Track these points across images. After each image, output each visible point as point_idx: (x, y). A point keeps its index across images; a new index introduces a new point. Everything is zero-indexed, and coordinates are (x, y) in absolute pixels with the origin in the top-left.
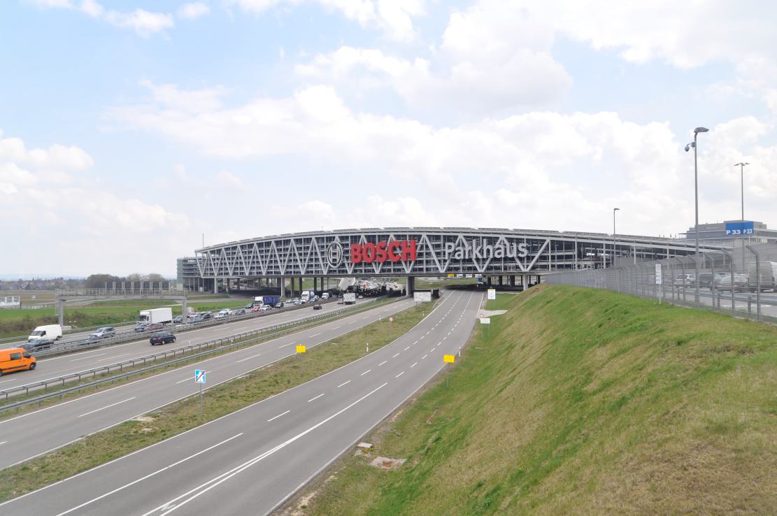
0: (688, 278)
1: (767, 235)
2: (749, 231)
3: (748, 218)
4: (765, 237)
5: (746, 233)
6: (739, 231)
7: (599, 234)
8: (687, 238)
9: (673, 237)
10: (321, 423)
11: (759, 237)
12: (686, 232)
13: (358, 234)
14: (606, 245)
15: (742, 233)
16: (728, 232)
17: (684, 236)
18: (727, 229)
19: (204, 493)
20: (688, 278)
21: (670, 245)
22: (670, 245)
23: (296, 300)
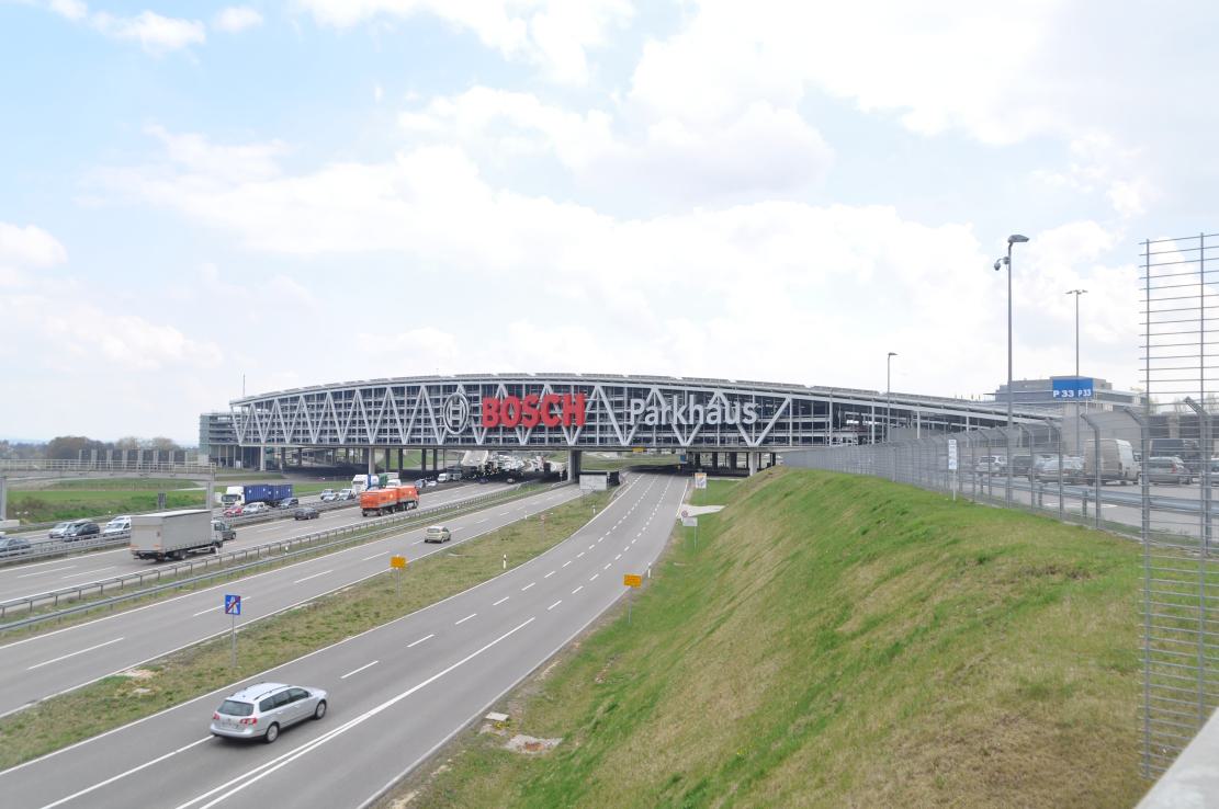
0: (997, 461)
1: (1113, 400)
2: (1087, 393)
3: (1084, 373)
5: (1082, 396)
6: (1072, 392)
7: (912, 396)
11: (1101, 402)
12: (994, 392)
15: (1076, 394)
16: (1056, 393)
17: (993, 398)
20: (997, 461)
21: (690, 386)
22: (690, 386)
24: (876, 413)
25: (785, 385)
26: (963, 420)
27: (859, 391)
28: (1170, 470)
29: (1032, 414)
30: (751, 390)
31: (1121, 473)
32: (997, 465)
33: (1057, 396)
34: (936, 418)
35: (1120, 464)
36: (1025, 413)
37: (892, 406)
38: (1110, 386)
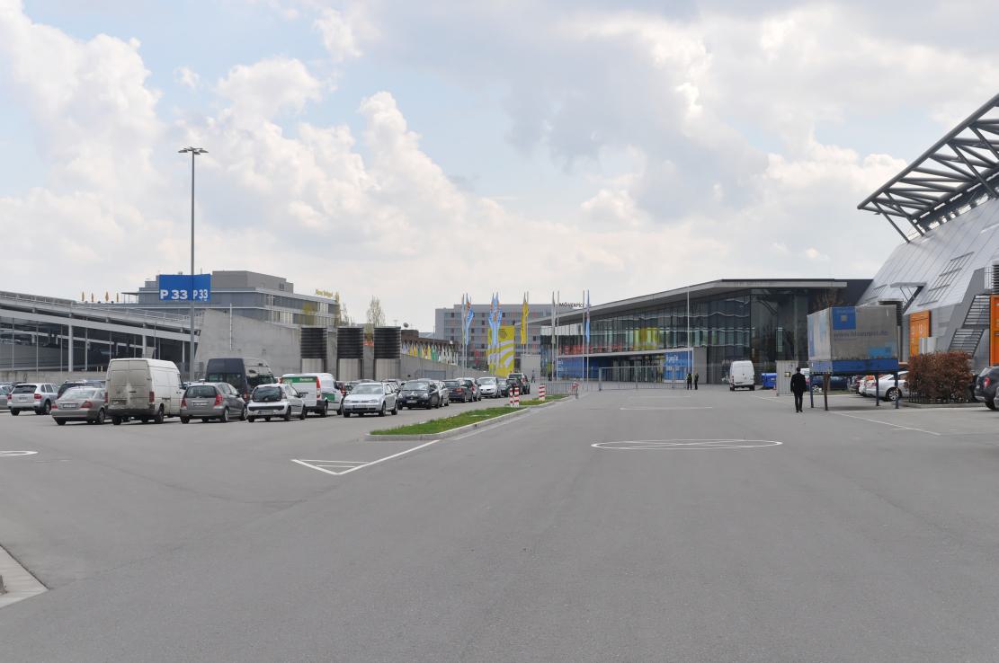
0: (38, 391)
1: (291, 306)
2: (204, 294)
3: (204, 267)
4: (289, 310)
5: (197, 298)
6: (185, 292)
7: (23, 297)
8: (140, 303)
9: (112, 298)
10: (375, 462)
11: (276, 308)
12: (137, 290)
13: (186, 338)
14: (75, 328)
15: (190, 296)
16: (164, 293)
17: (134, 299)
18: (161, 288)
19: (427, 447)
20: (38, 391)
21: (150, 327)
22: (150, 327)
23: (525, 398)
24: (75, 335)
25: (22, 296)
26: (139, 339)
27: (49, 300)
28: (213, 400)
29: (160, 323)
30: (139, 325)
31: (152, 407)
32: (38, 397)
33: (165, 298)
34: (30, 326)
35: (152, 394)
36: (150, 322)
37: (151, 333)
38: (291, 285)
